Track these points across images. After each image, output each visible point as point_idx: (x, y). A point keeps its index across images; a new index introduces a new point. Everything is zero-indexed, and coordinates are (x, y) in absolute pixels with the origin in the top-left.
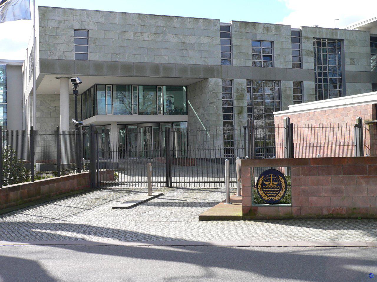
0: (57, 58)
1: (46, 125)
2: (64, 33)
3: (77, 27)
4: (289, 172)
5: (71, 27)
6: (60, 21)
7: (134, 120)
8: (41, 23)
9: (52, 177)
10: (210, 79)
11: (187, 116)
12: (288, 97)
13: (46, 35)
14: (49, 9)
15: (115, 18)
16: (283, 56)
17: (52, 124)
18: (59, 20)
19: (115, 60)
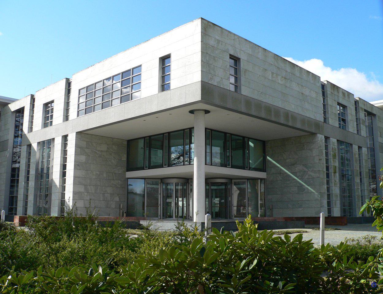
0: (216, 84)
1: (90, 173)
2: (222, 56)
3: (232, 53)
4: (306, 281)
5: (226, 51)
6: (218, 41)
7: (230, 174)
8: (203, 38)
9: (191, 245)
10: (318, 135)
11: (265, 173)
12: (146, 167)
13: (207, 53)
14: (210, 24)
15: (259, 52)
16: (232, 80)
17: (98, 172)
18: (217, 40)
19: (260, 99)
